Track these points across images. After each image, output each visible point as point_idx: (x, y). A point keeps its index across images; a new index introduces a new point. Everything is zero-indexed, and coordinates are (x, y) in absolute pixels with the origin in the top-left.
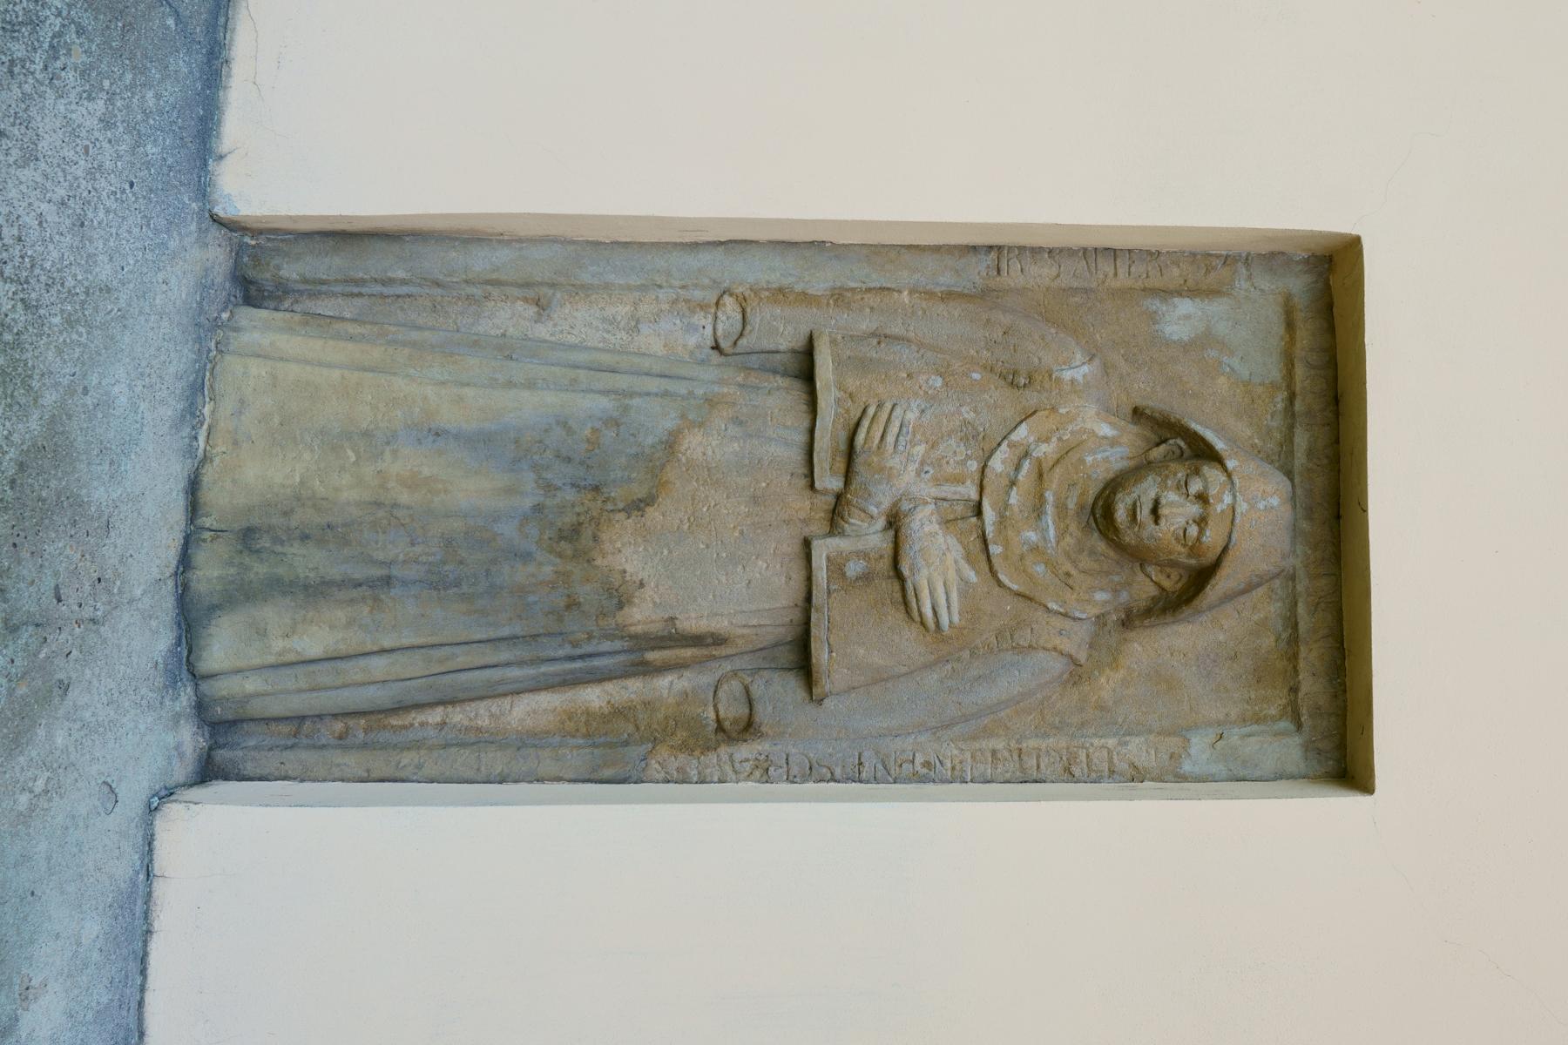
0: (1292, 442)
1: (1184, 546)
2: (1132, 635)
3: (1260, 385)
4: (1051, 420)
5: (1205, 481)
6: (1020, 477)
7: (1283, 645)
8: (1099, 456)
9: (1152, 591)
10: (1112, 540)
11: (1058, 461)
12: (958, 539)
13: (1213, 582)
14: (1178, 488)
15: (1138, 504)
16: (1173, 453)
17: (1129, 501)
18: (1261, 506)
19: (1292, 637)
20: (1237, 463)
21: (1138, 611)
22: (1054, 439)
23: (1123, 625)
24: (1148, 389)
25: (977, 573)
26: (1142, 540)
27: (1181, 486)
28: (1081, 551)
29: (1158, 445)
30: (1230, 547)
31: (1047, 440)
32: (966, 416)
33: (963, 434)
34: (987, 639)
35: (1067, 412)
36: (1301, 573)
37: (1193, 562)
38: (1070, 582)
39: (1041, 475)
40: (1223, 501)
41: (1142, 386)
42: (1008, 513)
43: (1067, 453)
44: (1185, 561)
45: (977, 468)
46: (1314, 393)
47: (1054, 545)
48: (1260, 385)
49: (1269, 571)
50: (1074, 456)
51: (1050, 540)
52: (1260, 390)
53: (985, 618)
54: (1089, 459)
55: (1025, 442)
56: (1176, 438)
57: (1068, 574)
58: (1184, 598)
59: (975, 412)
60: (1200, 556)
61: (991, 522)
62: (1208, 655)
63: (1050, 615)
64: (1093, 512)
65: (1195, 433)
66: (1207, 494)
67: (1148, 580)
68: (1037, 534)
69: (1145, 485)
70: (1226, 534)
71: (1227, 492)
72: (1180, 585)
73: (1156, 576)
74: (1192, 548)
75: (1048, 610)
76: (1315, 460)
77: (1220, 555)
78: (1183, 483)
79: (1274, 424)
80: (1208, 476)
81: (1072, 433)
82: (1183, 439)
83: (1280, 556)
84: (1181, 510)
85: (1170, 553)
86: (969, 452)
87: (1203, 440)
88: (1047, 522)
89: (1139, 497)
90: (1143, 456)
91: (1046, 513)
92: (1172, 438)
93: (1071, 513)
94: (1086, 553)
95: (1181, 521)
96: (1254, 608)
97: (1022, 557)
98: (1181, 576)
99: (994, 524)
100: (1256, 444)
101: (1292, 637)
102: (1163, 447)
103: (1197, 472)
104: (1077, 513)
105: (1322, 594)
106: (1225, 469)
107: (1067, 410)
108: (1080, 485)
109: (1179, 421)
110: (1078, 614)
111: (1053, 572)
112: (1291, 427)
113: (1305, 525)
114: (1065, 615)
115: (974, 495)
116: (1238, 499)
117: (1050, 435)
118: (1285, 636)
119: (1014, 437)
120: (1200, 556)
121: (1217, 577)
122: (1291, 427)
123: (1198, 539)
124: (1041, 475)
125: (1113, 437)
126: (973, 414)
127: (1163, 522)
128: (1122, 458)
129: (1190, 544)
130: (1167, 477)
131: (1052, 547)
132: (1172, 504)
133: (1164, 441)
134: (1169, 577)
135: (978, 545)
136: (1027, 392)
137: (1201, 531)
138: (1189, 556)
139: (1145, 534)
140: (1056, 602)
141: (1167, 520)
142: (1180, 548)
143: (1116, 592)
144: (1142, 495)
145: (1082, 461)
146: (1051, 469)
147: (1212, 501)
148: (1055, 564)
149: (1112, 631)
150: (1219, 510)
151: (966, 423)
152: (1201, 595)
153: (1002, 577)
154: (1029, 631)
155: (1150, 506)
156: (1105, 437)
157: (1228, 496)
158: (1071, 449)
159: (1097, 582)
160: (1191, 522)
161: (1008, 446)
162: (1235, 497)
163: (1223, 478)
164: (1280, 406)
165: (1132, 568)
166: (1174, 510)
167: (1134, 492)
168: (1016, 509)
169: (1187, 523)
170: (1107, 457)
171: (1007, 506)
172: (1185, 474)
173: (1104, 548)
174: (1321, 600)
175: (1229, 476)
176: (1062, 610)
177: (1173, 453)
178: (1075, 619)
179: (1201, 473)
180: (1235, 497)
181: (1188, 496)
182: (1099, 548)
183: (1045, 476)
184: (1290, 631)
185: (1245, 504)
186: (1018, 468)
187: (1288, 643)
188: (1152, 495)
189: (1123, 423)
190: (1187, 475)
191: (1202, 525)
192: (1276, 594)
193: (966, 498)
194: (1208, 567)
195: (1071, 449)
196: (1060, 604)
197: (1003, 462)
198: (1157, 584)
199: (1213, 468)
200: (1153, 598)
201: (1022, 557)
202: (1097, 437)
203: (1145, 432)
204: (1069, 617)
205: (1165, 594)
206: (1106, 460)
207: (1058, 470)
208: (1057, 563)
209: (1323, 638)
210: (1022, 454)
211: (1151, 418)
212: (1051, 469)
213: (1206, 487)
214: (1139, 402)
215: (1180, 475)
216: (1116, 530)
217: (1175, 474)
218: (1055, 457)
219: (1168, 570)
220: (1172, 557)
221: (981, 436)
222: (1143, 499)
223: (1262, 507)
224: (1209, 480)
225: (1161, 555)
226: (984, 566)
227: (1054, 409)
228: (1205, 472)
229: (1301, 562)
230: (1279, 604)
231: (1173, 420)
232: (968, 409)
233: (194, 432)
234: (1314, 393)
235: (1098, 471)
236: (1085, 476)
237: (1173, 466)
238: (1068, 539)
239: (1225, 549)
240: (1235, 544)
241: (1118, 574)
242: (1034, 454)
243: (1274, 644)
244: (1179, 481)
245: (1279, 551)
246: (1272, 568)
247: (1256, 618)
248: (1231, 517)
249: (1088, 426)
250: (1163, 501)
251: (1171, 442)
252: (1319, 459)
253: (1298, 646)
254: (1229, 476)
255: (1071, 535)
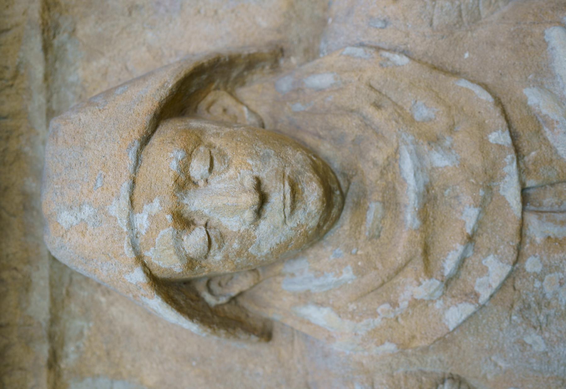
0: (53, 301)
1: (210, 146)
2: (270, 38)
3: (98, 376)
4: (407, 332)
5: (179, 250)
6: (460, 248)
7: (65, 24)
8: (331, 278)
9: (243, 92)
10: (315, 156)
11: (399, 271)
12: (556, 152)
13: (164, 93)
14: (222, 237)
15: (288, 210)
16: (220, 284)
17: (300, 215)
18: (87, 211)
19: (51, 34)
20: (127, 277)
21: (263, 67)
22: (404, 305)
23: (282, 50)
24: (251, 366)
25: (524, 103)
26: (277, 155)
27: (217, 240)
28: (356, 142)
29: (241, 294)
30: (137, 144)
31: (415, 303)
32: (538, 339)
33: (545, 311)
34: (492, 13)
35: (382, 343)
36: (39, 120)
37: (194, 124)
38: (374, 96)
39: (426, 252)
40: (150, 216)
41: (260, 370)
42: (481, 193)
43: (383, 283)
44: (207, 125)
45: (525, 261)
46: (21, 369)
47: (403, 147)
48: (98, 376)
49: (78, 112)
50: (371, 278)
51: (411, 153)
52: (98, 369)
53: (502, 40)
54: (348, 275)
55: (450, 300)
56: (217, 306)
57: (378, 106)
58: (204, 77)
59: (524, 344)
60: (185, 131)
61: (507, 179)
62: (167, 11)
63: (403, 47)
64: (343, 196)
65: (191, 317)
66: (175, 227)
67: (253, 107)
68: (431, 164)
69: (274, 241)
70: (144, 165)
71: (143, 232)
72: (210, 98)
73: (242, 112)
74: (199, 142)
75: (405, 53)
76: (20, 276)
77: (153, 132)
78: (215, 245)
79: (79, 323)
80: (175, 257)
81: (375, 314)
82: (207, 305)
83: (61, 134)
84: (220, 202)
85: (232, 136)
86: (537, 284)
87: (180, 309)
88: (417, 181)
89: (285, 222)
90: (261, 278)
91: (418, 194)
92: (222, 305)
93: (377, 196)
94: (350, 139)
95: (217, 184)
96: (105, 75)
97: (452, 129)
98: (208, 109)
99: (503, 177)
100: (104, 295)
101: (51, 34)
102: (234, 290)
103: (191, 263)
104: (365, 196)
105: (8, 91)
106: (145, 267)
107: (381, 348)
108: (363, 238)
109: (214, 332)
110: (360, 51)
111: (402, 108)
112: (54, 320)
113: (31, 184)
114: (378, 49)
115: (532, 220)
116: (125, 221)
117: (410, 311)
118: (63, 37)
119: (469, 308)
120: (185, 131)
121: (158, 99)
122: (54, 320)
123: (189, 155)
124: (426, 252)
125: (306, 304)
126: (528, 340)
127: (249, 183)
128: (293, 275)
129: (202, 148)
130: (239, 254)
131: (407, 145)
132: (235, 210)
133: (233, 299)
134: (225, 110)
135: (524, 145)
136: (439, 370)
137: (185, 167)
138: (202, 131)
139: (274, 162)
140: (395, 65)
141: (242, 184)
142: (218, 142)
143: (298, 89)
144: (280, 225)
145: (359, 272)
146: (410, 260)
147: (169, 217)
148: (400, 120)
149: (296, 43)
150: (156, 203)
151: (539, 328)
152: (182, 75)
153: (486, 97)
154: (436, 23)
155: (268, 208)
156: (320, 304)
157: (141, 225)
158: (377, 289)
159: (330, 99)
160: (201, 183)
161: (477, 295)
162: (130, 224)
163: (150, 255)
164: (70, 348)
165: (276, 122)
166: (231, 201)
167: (291, 229)
168: (466, 199)
169: (207, 181)
170: (317, 277)
171: (482, 206)
172: (210, 259)
173: (322, 147)
174: (10, 83)
175: (140, 259)
176: (386, 54)
177: (220, 284)
178: (362, 45)
179: (186, 261)
180: (130, 224)
181: (206, 225)
182: (329, 146)
183: (420, 250)
184: (56, 42)
185: (113, 213)
186: (462, 262)
187: (57, 26)
188: (264, 225)
189: (289, 322)
190: (206, 257)
191: (183, 178)
192: (75, 93)
193: (544, 215)
194: (171, 116)
195: (377, 289)
196: (389, 63)
197: (484, 271)
198: (240, 102)
199: (166, 270)
200: (243, 84)
201: (452, 129)
202: (333, 307)
203: (256, 309)
204: (371, 47)
205: (229, 89)
206: (319, 273)
207: (400, 260)
208: (397, 122)
209: (7, 30)
210: (453, 283)
211: (250, 330)
212: (410, 260)
213: (178, 239)
214: (264, 349)
215: (219, 257)
216: (316, 169)
217: (226, 258)
218: (401, 279)
219: (226, 118)
220: (228, 130)
221: (517, 308)
222: (279, 218)
223: (86, 208)
224: (172, 252)
225: (245, 133)
226: (515, 114)
227: (403, 347)
228: (179, 264)
229: (38, 134)
230: (72, 79)
231: (222, 331)
232: (535, 348)
233: (217, 230)
234: (21, 369)
235: (332, 258)
236: (354, 251)
237: (227, 269)
238: (381, 158)
239: (145, 140)
240: (129, 148)
241: (296, 113)
242: (438, 283)
243: (79, 27)
244: (220, 248)
245: (60, 141)
246: (72, 116)
247: (103, 61)
248: (136, 191)
249: (347, 325)
250: (249, 215)
251: (223, 300)
252: (14, 278)
253: (42, 18)
254: (140, 259)
255: (375, 164)
